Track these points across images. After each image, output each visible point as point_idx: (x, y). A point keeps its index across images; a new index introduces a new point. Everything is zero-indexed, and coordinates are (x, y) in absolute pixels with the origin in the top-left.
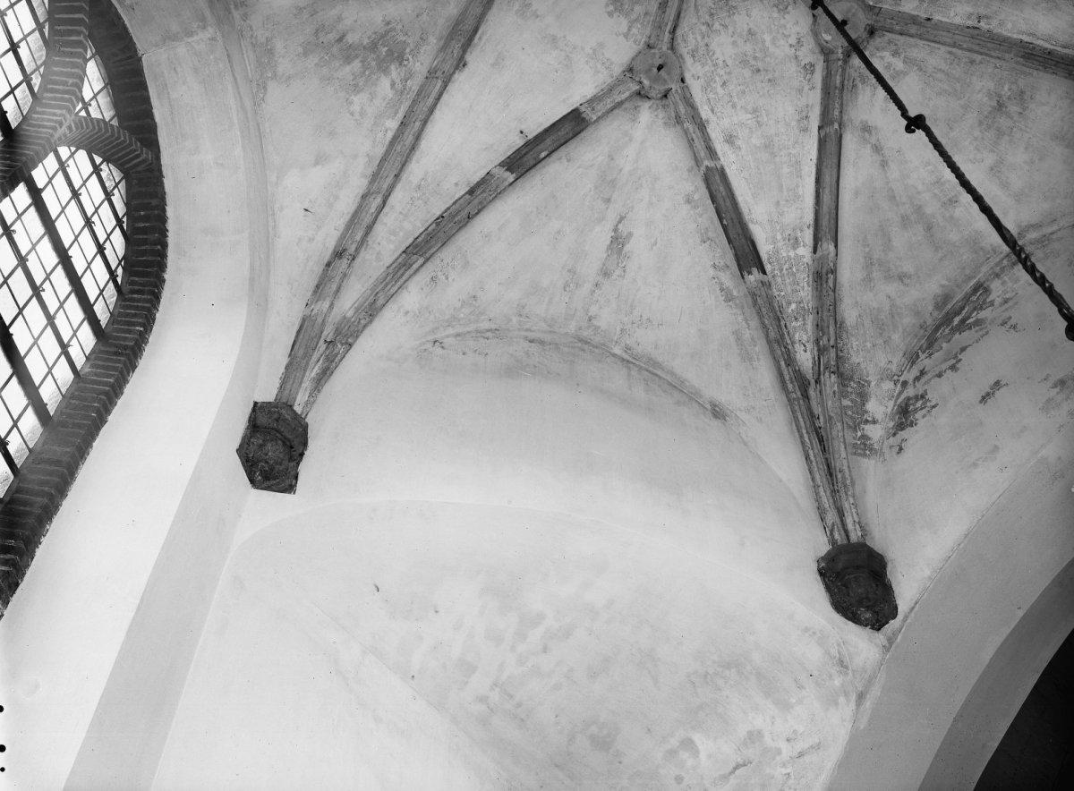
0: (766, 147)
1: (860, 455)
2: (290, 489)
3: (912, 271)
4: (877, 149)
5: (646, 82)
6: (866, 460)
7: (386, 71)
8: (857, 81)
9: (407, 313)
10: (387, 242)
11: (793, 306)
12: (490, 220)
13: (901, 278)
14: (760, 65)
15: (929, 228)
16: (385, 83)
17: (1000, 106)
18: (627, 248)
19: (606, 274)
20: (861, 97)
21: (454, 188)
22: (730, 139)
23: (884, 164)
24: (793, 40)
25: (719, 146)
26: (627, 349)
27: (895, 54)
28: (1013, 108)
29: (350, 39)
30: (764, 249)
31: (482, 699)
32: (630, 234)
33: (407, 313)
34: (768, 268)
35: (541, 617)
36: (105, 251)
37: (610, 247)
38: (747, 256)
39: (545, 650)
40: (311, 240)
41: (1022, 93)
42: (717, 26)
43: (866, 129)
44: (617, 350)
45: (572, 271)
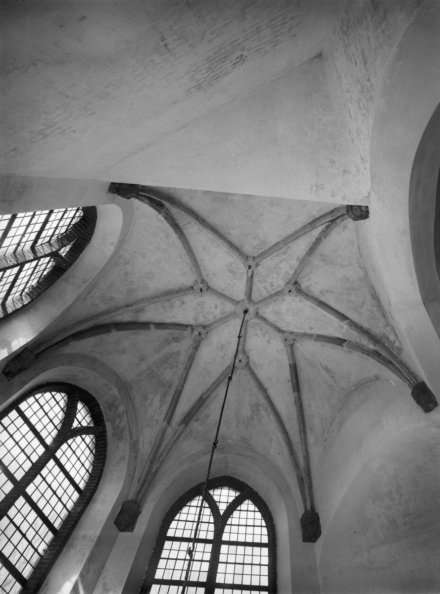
0: (316, 321)
1: (401, 354)
2: (304, 541)
3: (362, 300)
4: (327, 291)
5: (289, 344)
6: (402, 354)
7: (260, 411)
8: (308, 289)
9: (314, 444)
10: (295, 437)
11: (358, 339)
12: (305, 403)
13: (363, 303)
14: (296, 312)
15: (353, 289)
16: (262, 412)
17: (324, 260)
18: (329, 367)
19: (333, 377)
20: (313, 291)
21: (293, 409)
22: (311, 328)
23: (332, 292)
24: (292, 301)
25: (312, 332)
26: (353, 385)
27: (304, 278)
28: (325, 258)
29: (249, 416)
30: (341, 336)
31: (405, 523)
32: (326, 365)
33: (314, 444)
34: (346, 338)
35: (390, 490)
36: (404, 357)
37: (327, 372)
38: (340, 342)
39: (401, 495)
40: (285, 459)
41: (321, 255)
42: (283, 318)
43: (321, 292)
44: (353, 388)
45: (329, 386)
